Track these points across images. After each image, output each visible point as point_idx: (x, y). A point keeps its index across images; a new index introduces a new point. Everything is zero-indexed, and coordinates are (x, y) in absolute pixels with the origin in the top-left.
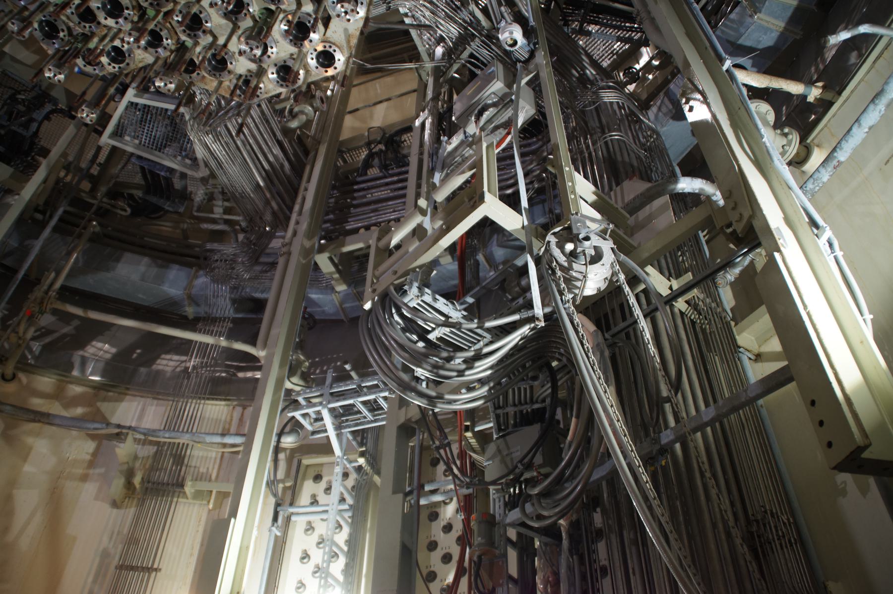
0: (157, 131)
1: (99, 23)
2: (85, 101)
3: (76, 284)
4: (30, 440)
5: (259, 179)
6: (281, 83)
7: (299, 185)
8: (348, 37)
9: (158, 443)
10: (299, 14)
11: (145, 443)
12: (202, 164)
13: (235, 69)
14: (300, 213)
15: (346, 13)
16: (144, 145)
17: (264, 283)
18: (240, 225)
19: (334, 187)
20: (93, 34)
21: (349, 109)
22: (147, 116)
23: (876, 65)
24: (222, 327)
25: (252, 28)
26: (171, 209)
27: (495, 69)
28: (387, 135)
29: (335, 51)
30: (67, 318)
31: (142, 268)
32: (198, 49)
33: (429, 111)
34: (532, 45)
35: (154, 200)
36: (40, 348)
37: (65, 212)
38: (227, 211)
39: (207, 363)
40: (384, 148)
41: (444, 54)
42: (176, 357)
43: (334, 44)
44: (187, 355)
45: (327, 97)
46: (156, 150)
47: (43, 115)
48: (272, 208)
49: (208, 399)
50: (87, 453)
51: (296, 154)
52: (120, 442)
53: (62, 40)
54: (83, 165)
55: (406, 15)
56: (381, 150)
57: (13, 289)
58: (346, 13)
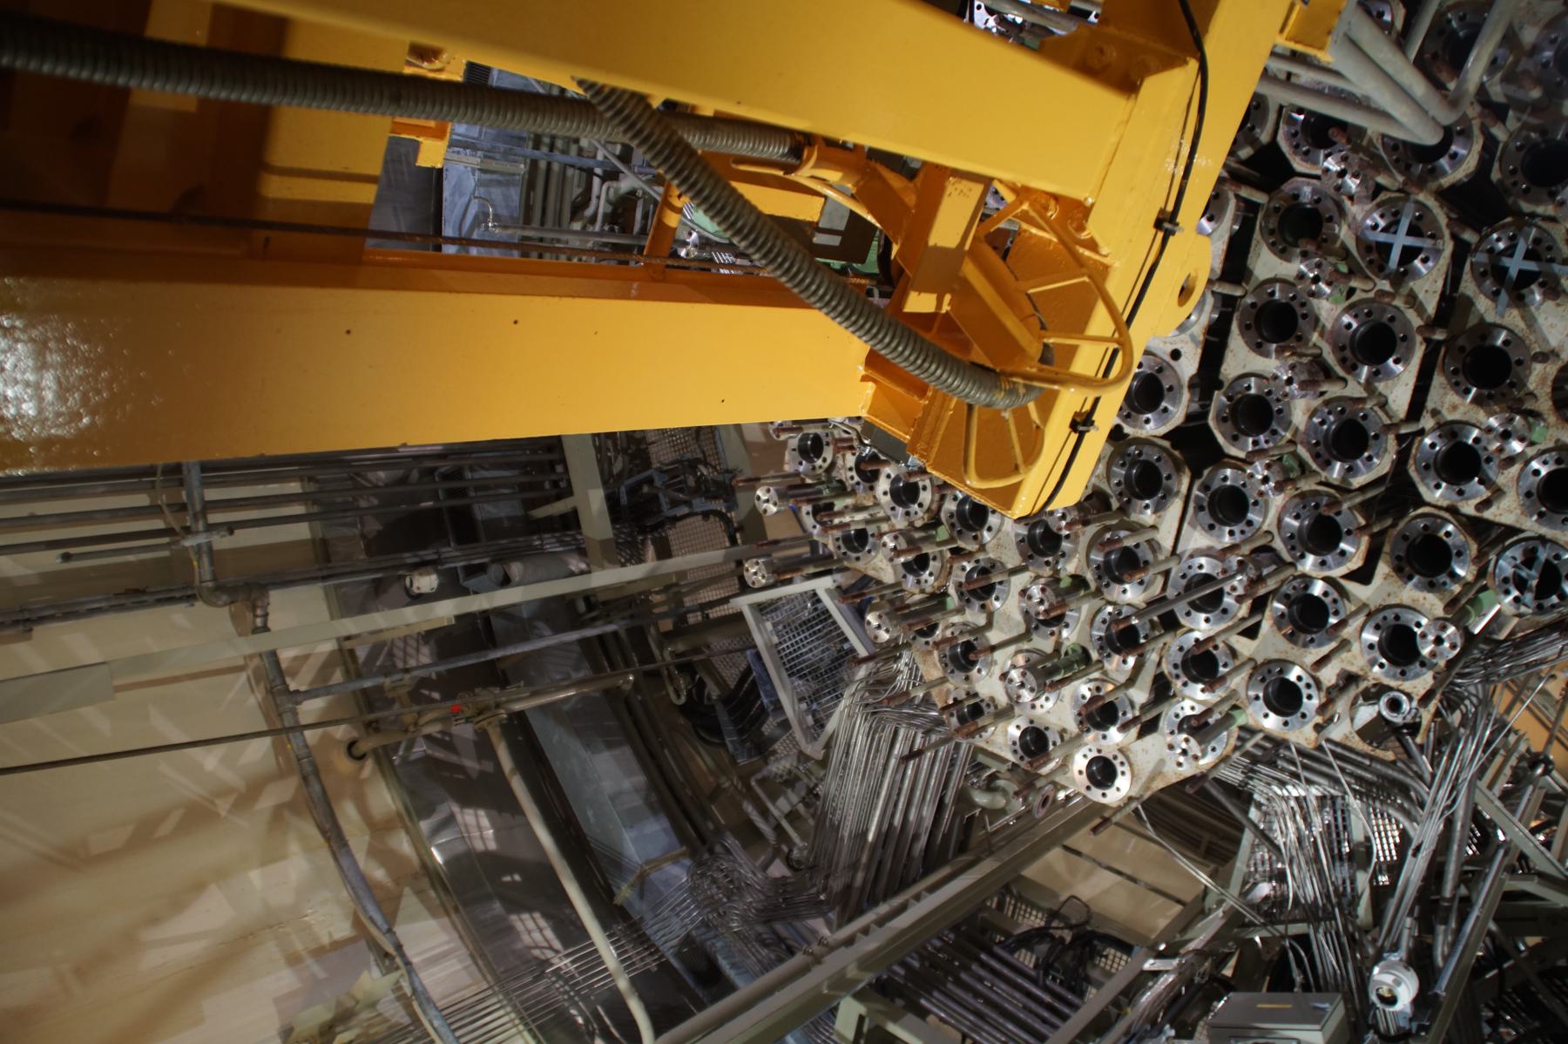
0: (811, 650)
1: (872, 488)
2: (768, 555)
3: (536, 723)
4: (294, 847)
5: (873, 828)
6: (1018, 747)
7: (915, 881)
8: (1157, 773)
9: (416, 1020)
10: (1120, 694)
11: (402, 998)
12: (823, 739)
13: (978, 680)
14: (881, 922)
15: (1184, 752)
16: (779, 652)
17: (748, 957)
18: (791, 851)
19: (955, 928)
20: (853, 493)
21: (1070, 842)
22: (817, 624)
24: (642, 959)
25: (1048, 657)
26: (730, 747)
27: (1330, 1010)
28: (1089, 928)
29: (1123, 773)
30: (484, 748)
31: (627, 784)
32: (956, 619)
33: (1180, 965)
34: (1414, 1026)
35: (723, 717)
36: (422, 754)
37: (615, 634)
38: (792, 816)
39: (578, 983)
40: (1068, 939)
41: (1267, 898)
42: (549, 934)
43: (1131, 765)
44: (566, 946)
45: (1055, 800)
46: (787, 670)
47: (706, 508)
48: (853, 878)
49: (530, 1031)
50: (330, 934)
51: (947, 836)
52: (378, 965)
53: (814, 468)
54: (688, 602)
55: (1259, 806)
56: (1062, 939)
57: (470, 662)
58: (1184, 752)
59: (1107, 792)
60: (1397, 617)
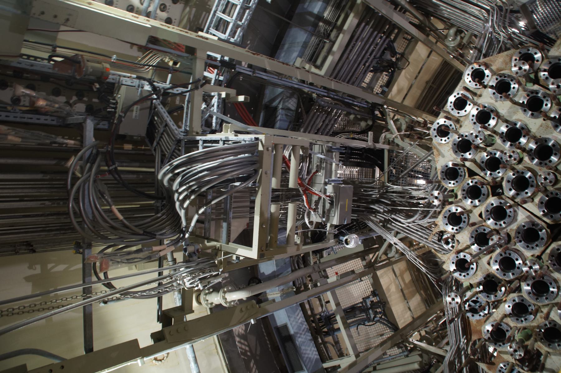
23: (214, 345)
59: (438, 137)
60: (461, 176)
